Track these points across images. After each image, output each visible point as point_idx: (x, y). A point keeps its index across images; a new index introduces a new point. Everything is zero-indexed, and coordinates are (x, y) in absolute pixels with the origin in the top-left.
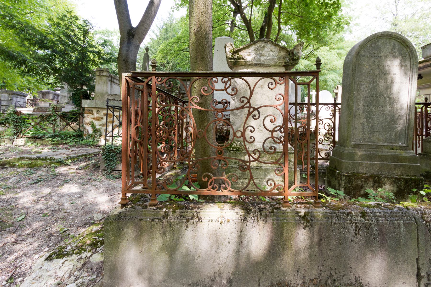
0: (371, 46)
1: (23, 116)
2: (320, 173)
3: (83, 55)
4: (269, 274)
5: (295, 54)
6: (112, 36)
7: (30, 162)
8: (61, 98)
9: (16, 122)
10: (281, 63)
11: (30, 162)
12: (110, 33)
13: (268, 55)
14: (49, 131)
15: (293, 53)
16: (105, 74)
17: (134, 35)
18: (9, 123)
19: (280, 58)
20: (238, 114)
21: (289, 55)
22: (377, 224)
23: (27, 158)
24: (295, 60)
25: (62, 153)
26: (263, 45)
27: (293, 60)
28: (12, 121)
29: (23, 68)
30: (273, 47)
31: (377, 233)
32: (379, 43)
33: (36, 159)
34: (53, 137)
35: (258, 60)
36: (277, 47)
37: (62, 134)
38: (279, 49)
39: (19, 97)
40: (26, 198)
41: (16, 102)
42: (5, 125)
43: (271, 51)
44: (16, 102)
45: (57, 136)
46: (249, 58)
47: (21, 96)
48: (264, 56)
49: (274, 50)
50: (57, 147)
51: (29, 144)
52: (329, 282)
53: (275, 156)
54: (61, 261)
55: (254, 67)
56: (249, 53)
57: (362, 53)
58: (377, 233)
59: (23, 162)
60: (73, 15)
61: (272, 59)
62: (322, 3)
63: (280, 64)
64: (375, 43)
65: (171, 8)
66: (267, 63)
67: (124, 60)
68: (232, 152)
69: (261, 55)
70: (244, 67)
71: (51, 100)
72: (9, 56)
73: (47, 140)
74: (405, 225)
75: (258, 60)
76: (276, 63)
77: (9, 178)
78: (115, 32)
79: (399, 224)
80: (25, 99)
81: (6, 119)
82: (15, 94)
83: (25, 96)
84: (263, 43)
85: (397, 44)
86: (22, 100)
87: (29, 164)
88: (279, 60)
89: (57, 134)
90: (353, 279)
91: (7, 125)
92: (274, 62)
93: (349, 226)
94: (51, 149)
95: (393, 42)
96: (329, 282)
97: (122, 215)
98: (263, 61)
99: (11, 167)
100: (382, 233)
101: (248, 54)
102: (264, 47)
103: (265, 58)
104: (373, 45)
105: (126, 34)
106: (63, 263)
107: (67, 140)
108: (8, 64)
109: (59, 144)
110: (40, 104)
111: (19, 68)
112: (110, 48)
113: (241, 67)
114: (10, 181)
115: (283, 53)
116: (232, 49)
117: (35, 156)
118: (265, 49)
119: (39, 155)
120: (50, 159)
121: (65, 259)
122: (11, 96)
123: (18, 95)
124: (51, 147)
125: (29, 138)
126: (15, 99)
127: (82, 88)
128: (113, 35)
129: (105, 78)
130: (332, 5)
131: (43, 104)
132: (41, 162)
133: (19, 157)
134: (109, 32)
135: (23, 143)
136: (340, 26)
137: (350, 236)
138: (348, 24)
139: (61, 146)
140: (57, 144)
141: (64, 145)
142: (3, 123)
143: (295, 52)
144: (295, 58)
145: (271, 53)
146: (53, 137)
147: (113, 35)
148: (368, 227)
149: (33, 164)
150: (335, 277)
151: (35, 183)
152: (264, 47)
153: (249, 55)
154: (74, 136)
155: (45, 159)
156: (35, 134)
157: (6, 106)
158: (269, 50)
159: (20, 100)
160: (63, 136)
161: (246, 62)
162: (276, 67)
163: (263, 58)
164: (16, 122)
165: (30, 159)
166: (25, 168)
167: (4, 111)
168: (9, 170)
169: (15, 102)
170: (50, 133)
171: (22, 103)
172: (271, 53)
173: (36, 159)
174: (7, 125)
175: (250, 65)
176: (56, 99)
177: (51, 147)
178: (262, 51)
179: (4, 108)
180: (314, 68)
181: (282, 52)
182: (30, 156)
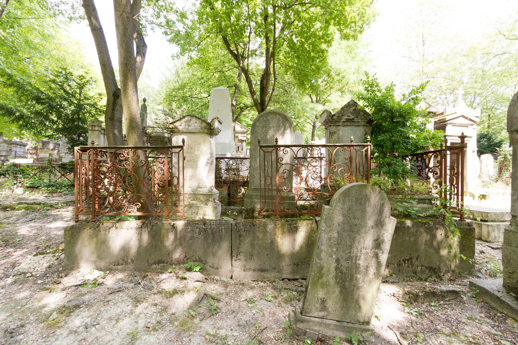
0: (263, 119)
1: (22, 168)
3: (80, 107)
4: (153, 256)
7: (27, 205)
8: (62, 148)
9: (16, 174)
11: (27, 205)
14: (45, 181)
16: (97, 128)
17: (119, 96)
18: (8, 174)
22: (210, 229)
23: (25, 203)
25: (56, 199)
28: (12, 172)
29: (21, 122)
31: (210, 233)
32: (269, 117)
33: (32, 204)
34: (49, 186)
35: (188, 129)
37: (57, 184)
39: (18, 146)
40: (24, 230)
41: (16, 152)
42: (5, 176)
43: (196, 123)
44: (16, 152)
45: (52, 186)
46: (181, 128)
47: (21, 145)
49: (197, 122)
50: (52, 195)
51: (27, 193)
52: (185, 260)
54: (42, 256)
57: (258, 124)
58: (210, 233)
59: (22, 206)
60: (68, 71)
61: (196, 129)
64: (266, 118)
65: (172, 56)
66: (193, 131)
67: (110, 118)
71: (52, 150)
72: (9, 112)
73: (43, 189)
74: (225, 229)
75: (188, 129)
77: (11, 217)
79: (222, 228)
80: (25, 149)
81: (7, 171)
82: (14, 144)
83: (25, 146)
85: (281, 118)
86: (22, 150)
87: (26, 207)
89: (52, 183)
90: (198, 258)
91: (7, 176)
93: (196, 230)
94: (46, 197)
95: (278, 117)
96: (185, 260)
97: (74, 227)
99: (11, 210)
100: (213, 233)
103: (192, 128)
104: (265, 119)
105: (111, 95)
106: (44, 257)
107: (61, 189)
108: (6, 119)
109: (54, 193)
110: (40, 155)
111: (18, 122)
114: (12, 219)
117: (32, 202)
119: (34, 201)
120: (44, 204)
121: (45, 255)
122: (10, 146)
123: (17, 144)
124: (46, 195)
125: (28, 187)
126: (14, 149)
127: (79, 139)
129: (97, 132)
131: (42, 155)
132: (36, 206)
133: (18, 202)
135: (22, 192)
137: (196, 235)
139: (55, 195)
140: (52, 193)
141: (115, 218)
142: (3, 175)
145: (196, 125)
146: (49, 186)
148: (206, 230)
149: (31, 207)
150: (188, 257)
151: (30, 221)
153: (181, 126)
154: (68, 185)
155: (40, 204)
156: (33, 184)
157: (5, 156)
159: (19, 150)
160: (58, 185)
161: (179, 130)
163: (190, 128)
164: (16, 174)
165: (28, 204)
166: (23, 210)
167: (3, 161)
168: (10, 212)
169: (14, 152)
170: (46, 183)
171: (23, 153)
173: (32, 204)
174: (7, 176)
175: (182, 132)
176: (57, 149)
177: (46, 195)
179: (2, 158)
180: (181, 144)
182: (28, 202)
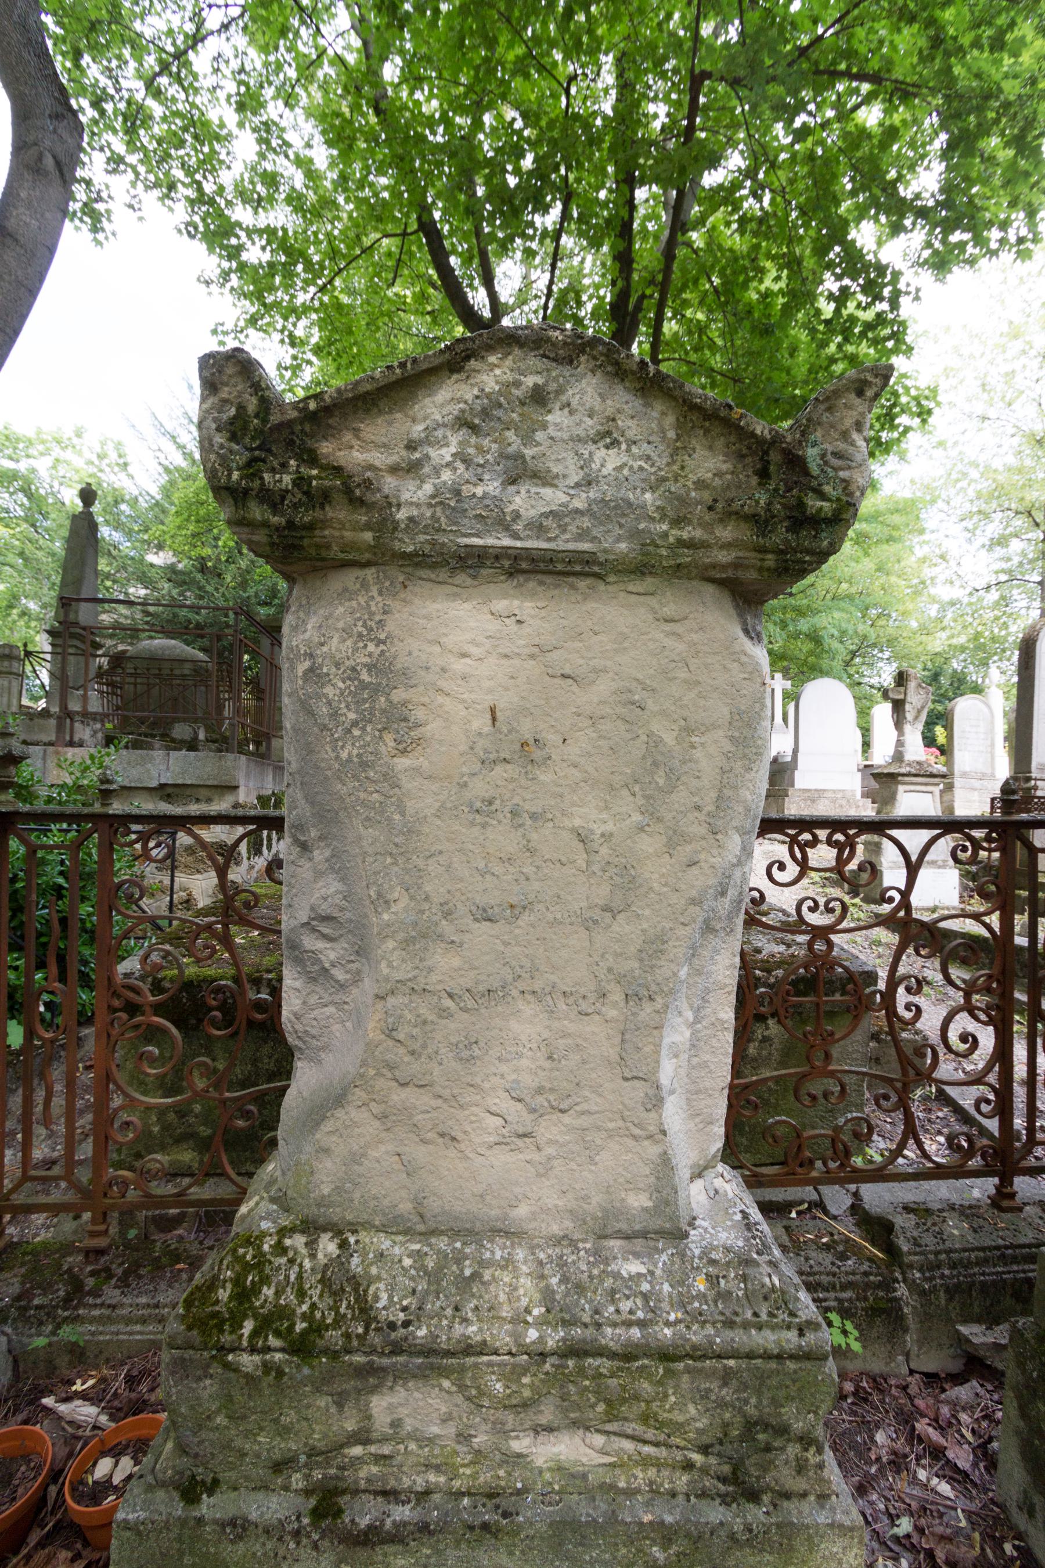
2: (934, 1289)
5: (814, 469)
6: (28, 456)
10: (690, 544)
12: (21, 446)
13: (575, 478)
15: (795, 462)
19: (682, 501)
20: (339, 974)
21: (764, 474)
24: (816, 522)
26: (530, 381)
27: (801, 520)
30: (622, 401)
36: (659, 406)
38: (679, 426)
43: (608, 436)
48: (542, 478)
49: (631, 427)
53: (646, 1387)
55: (461, 578)
56: (411, 446)
62: (827, 322)
63: (686, 557)
65: (215, 332)
66: (565, 543)
68: (248, 1361)
69: (519, 472)
70: (370, 573)
76: (647, 544)
78: (43, 442)
84: (533, 361)
88: (678, 522)
92: (634, 534)
98: (538, 528)
101: (398, 455)
102: (539, 398)
103: (554, 497)
112: (25, 501)
113: (350, 578)
115: (709, 463)
116: (252, 405)
118: (555, 416)
128: (32, 451)
130: (869, 326)
134: (18, 440)
136: (892, 420)
138: (924, 414)
143: (811, 453)
144: (814, 503)
145: (608, 461)
147: (32, 451)
152: (539, 398)
158: (591, 425)
162: (649, 583)
163: (525, 502)
172: (601, 453)
178: (528, 439)
181: (700, 452)
